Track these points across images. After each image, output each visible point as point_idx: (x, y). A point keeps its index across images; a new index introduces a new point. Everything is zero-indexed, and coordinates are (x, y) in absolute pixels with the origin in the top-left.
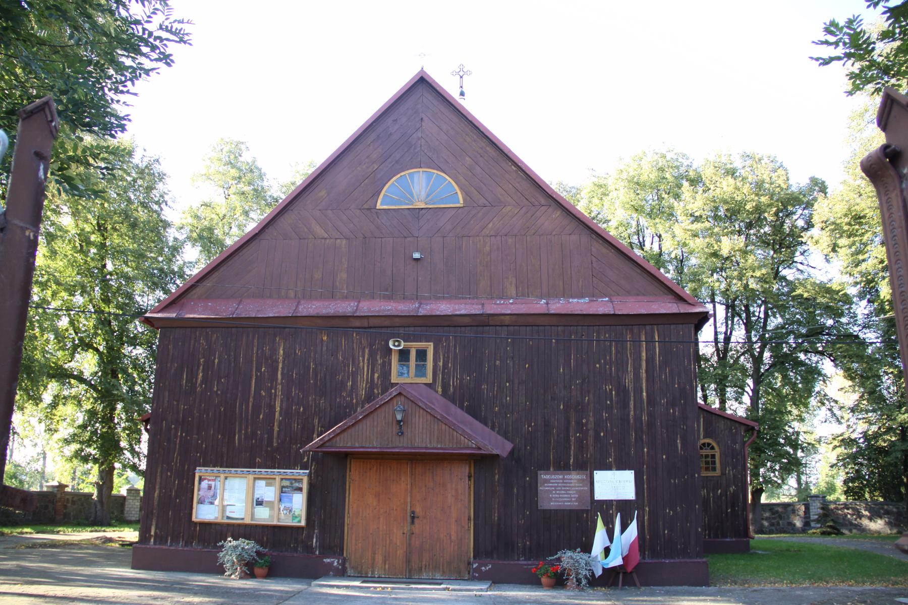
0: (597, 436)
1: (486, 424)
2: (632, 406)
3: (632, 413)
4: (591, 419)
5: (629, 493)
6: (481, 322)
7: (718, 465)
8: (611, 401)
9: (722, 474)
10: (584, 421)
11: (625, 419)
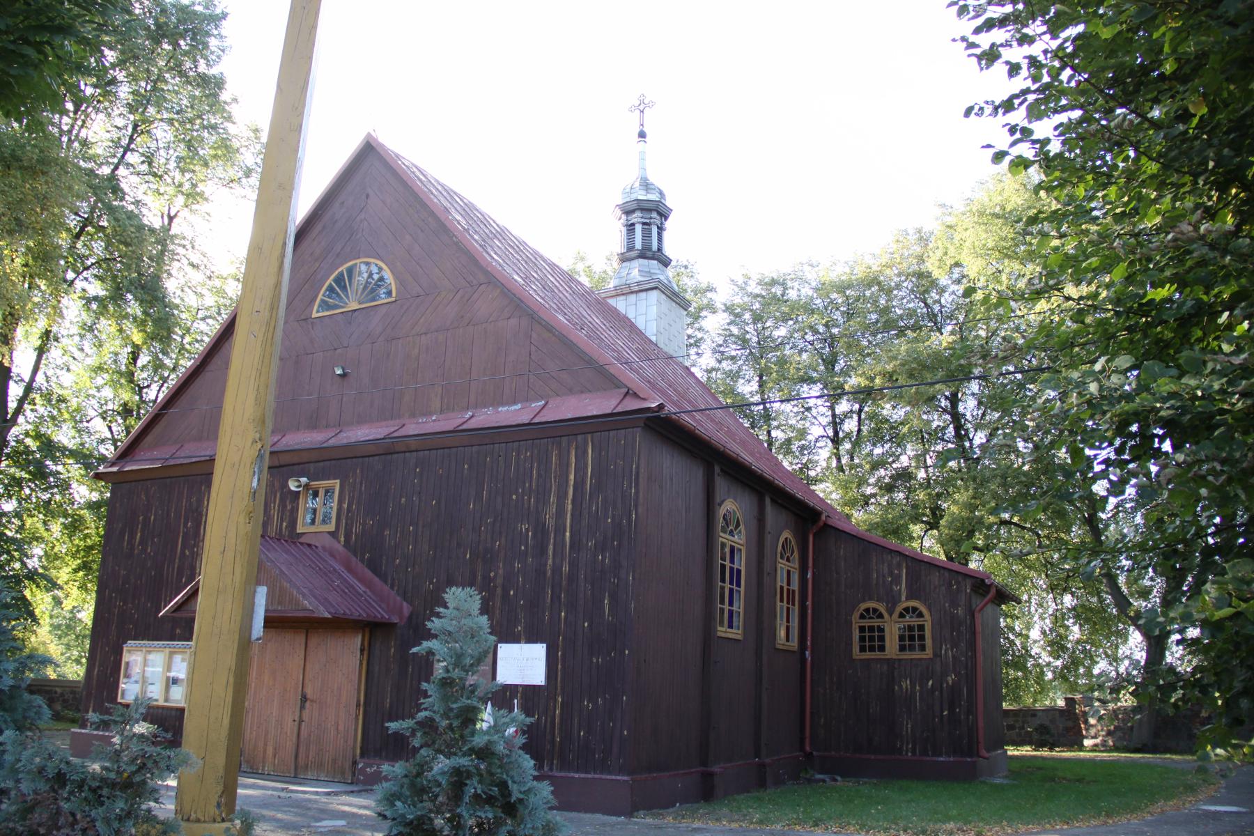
0: (505, 594)
1: (386, 582)
2: (551, 553)
3: (550, 562)
4: (501, 571)
5: (537, 676)
6: (388, 450)
7: (928, 642)
8: (526, 547)
9: (935, 655)
10: (492, 574)
11: (540, 571)
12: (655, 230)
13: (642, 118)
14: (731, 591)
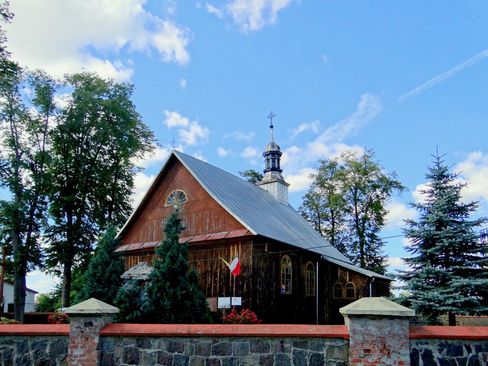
12: (276, 160)
13: (271, 121)
14: (310, 285)
